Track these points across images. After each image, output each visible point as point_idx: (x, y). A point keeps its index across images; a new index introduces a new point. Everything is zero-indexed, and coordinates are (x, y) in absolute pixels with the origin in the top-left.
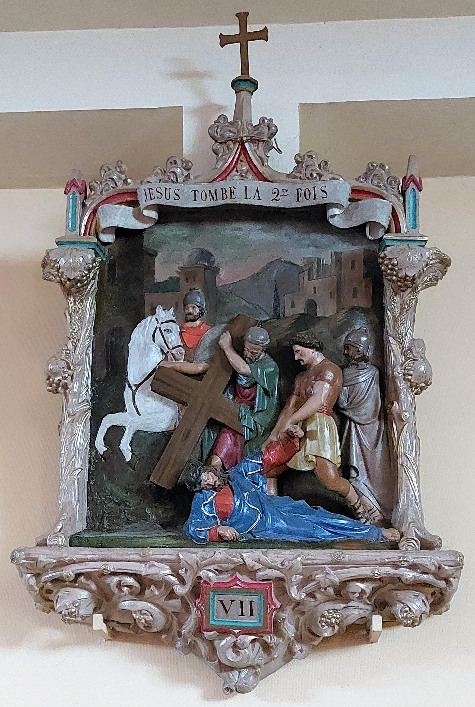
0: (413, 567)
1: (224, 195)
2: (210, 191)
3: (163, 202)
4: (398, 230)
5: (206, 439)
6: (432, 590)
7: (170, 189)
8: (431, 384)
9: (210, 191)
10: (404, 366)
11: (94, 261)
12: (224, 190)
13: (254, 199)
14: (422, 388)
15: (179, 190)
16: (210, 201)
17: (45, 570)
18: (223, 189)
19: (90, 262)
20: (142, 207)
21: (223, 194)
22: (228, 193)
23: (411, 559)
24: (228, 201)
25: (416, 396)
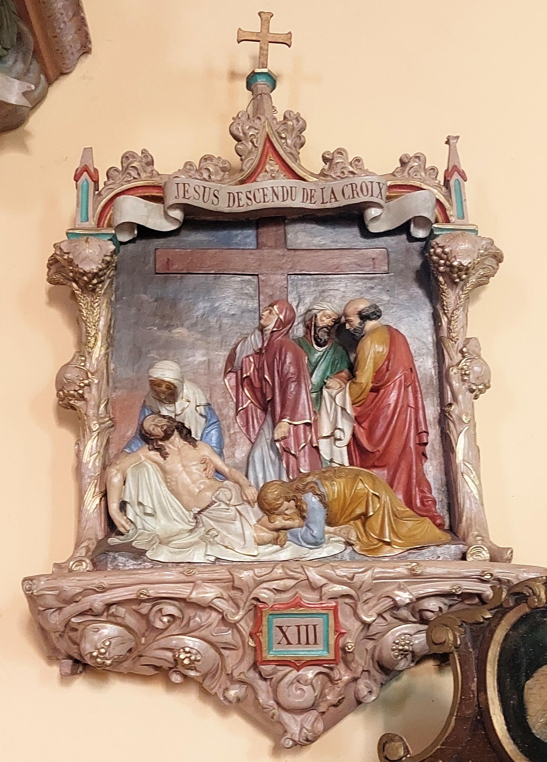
10: (460, 366)
14: (481, 391)
17: (72, 600)
19: (109, 254)
21: (353, 191)
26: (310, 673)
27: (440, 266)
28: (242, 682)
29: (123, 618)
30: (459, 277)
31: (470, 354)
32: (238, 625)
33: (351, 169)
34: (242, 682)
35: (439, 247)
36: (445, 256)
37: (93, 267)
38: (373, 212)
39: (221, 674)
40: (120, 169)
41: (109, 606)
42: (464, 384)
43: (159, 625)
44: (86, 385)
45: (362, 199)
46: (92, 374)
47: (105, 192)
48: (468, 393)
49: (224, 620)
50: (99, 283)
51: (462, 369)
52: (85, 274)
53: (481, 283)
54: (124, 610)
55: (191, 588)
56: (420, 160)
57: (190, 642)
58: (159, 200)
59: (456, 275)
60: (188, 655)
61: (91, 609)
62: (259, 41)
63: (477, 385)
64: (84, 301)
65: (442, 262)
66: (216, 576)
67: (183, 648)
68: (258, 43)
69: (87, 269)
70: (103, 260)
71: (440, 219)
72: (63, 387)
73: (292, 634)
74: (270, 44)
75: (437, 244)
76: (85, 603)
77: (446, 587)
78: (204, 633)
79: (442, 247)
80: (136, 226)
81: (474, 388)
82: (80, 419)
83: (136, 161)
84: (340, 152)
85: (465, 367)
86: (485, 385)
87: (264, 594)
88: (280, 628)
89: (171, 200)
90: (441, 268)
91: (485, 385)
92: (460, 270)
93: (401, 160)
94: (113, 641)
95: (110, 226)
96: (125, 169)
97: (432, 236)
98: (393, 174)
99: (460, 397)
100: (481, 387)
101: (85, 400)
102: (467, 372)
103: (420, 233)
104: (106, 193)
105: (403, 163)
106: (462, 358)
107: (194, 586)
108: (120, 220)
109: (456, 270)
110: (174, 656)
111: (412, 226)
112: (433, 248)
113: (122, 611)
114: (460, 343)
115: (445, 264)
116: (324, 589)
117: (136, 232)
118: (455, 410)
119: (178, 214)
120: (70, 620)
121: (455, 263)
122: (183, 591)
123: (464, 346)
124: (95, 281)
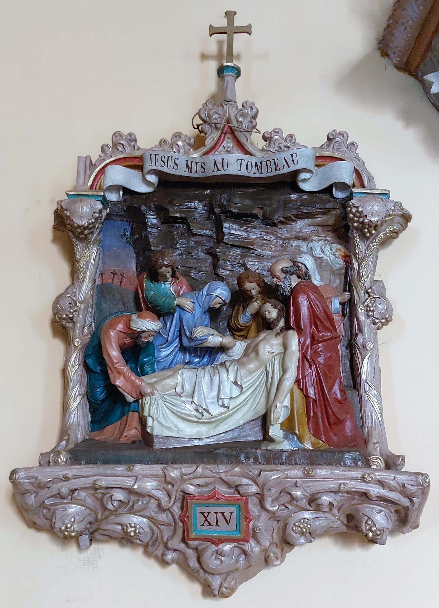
0: (382, 484)
1: (269, 169)
2: (256, 162)
3: (165, 169)
4: (363, 186)
5: (321, 396)
6: (397, 508)
7: (172, 157)
8: (391, 320)
9: (256, 162)
10: (366, 303)
11: (100, 211)
12: (268, 162)
13: (283, 169)
14: (383, 324)
15: (178, 159)
16: (255, 173)
18: (268, 162)
19: (98, 211)
20: (145, 171)
22: (273, 166)
23: (378, 475)
24: (274, 173)
25: (377, 331)
26: (227, 547)
27: (355, 222)
28: (175, 550)
29: (85, 500)
30: (370, 232)
31: (375, 294)
32: (171, 509)
33: (287, 144)
34: (175, 550)
35: (354, 207)
36: (358, 214)
37: (84, 222)
38: (303, 176)
39: (160, 543)
40: (111, 145)
41: (73, 491)
42: (367, 319)
43: (110, 507)
44: (75, 311)
45: (293, 168)
46: (80, 303)
47: (98, 162)
48: (372, 326)
49: (159, 505)
50: (90, 233)
51: (367, 306)
52: (79, 226)
53: (384, 243)
54: (84, 494)
55: (134, 480)
56: (343, 137)
57: (136, 519)
58: (140, 168)
59: (366, 230)
60: (133, 529)
61: (59, 494)
62: (226, 33)
63: (379, 319)
64: (79, 247)
65: (356, 219)
66: (154, 473)
67: (130, 524)
68: (226, 34)
69: (80, 223)
70: (93, 216)
71: (357, 183)
72: (58, 312)
73: (212, 518)
74: (235, 34)
75: (353, 204)
76: (55, 489)
77: (333, 485)
78: (147, 513)
79: (357, 207)
80: (121, 187)
81: (377, 321)
82: (108, 293)
83: (122, 139)
84: (276, 132)
85: (370, 305)
86: (386, 319)
87: (191, 489)
88: (202, 513)
89: (148, 167)
90: (355, 224)
91: (386, 319)
92: (370, 226)
93: (328, 137)
94: (77, 518)
95: (101, 188)
96: (115, 145)
97: (350, 197)
98: (322, 147)
99: (365, 330)
100: (383, 321)
101: (74, 323)
102: (372, 309)
103: (339, 195)
104: (99, 163)
105: (329, 139)
106: (368, 297)
107: (136, 480)
108: (108, 183)
109: (367, 226)
110: (123, 529)
111: (334, 189)
112: (351, 208)
113: (83, 494)
114: (368, 284)
115: (358, 221)
116: (135, 501)
117: (121, 193)
118: (360, 339)
119: (153, 179)
120: (43, 502)
121: (366, 221)
122: (128, 482)
123: (371, 288)
124: (86, 232)
